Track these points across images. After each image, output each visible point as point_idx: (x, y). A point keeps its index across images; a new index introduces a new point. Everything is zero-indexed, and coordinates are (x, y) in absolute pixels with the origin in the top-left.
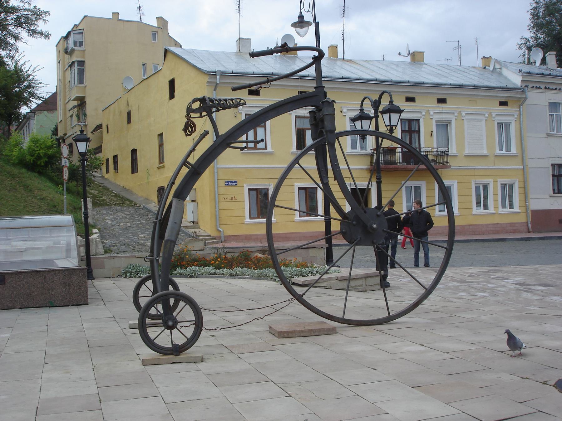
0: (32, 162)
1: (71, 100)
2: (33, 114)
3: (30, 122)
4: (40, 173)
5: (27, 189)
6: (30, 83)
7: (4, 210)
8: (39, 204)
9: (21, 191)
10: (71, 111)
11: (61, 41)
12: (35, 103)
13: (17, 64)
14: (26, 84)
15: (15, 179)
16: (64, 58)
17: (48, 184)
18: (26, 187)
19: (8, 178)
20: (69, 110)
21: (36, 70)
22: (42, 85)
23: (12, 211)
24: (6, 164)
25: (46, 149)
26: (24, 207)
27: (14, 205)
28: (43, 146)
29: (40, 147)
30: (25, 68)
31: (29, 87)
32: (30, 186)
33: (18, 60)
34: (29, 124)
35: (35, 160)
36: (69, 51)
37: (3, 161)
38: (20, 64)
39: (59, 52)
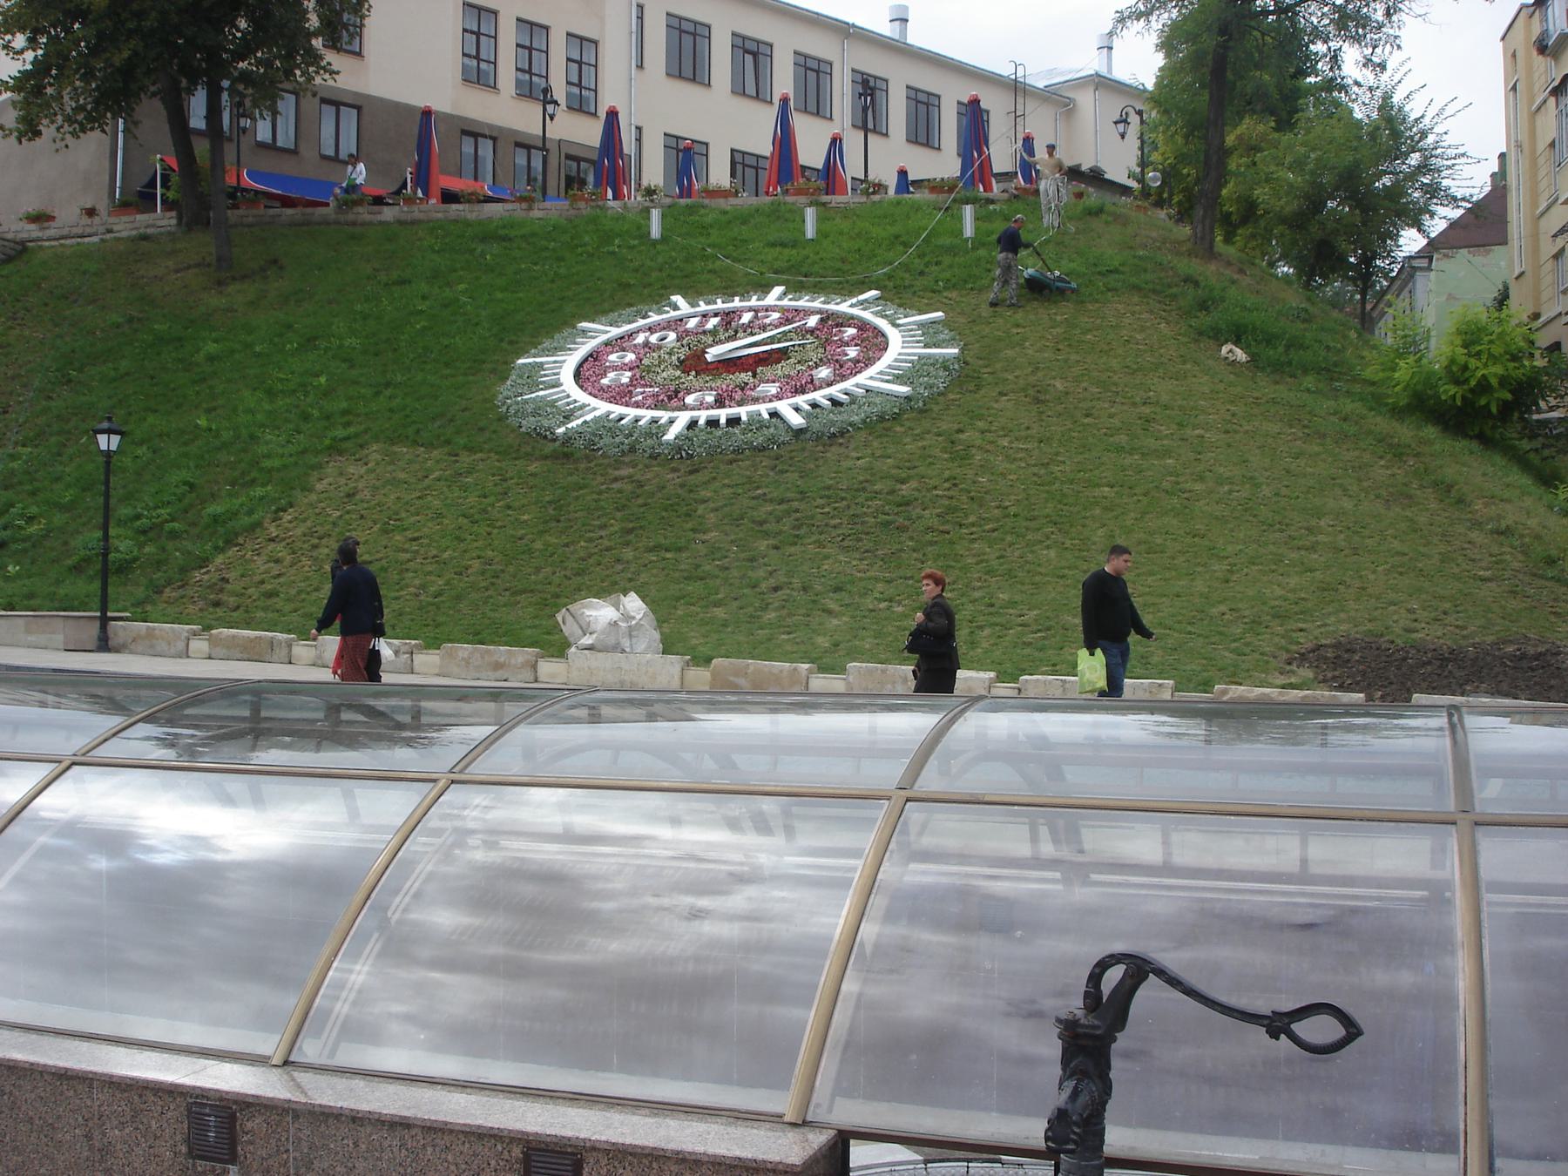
0: (1459, 403)
1: (1560, 201)
2: (1427, 260)
3: (1414, 284)
4: (1485, 440)
5: (1448, 497)
6: (1426, 158)
7: (1374, 572)
8: (1495, 549)
9: (1426, 502)
10: (1559, 239)
11: (1517, 20)
12: (1444, 218)
13: (1387, 97)
14: (1414, 159)
15: (1405, 462)
16: (1530, 70)
17: (1516, 478)
18: (1445, 489)
19: (1381, 458)
20: (1555, 236)
21: (1446, 114)
22: (1463, 160)
23: (1401, 574)
24: (1371, 409)
25: (1508, 360)
26: (1442, 562)
27: (1406, 555)
28: (1497, 350)
29: (1489, 353)
30: (1414, 110)
31: (1423, 168)
32: (1456, 487)
33: (1389, 87)
34: (1410, 292)
35: (1470, 396)
36: (1550, 43)
37: (1362, 400)
38: (1396, 99)
39: (1514, 55)
